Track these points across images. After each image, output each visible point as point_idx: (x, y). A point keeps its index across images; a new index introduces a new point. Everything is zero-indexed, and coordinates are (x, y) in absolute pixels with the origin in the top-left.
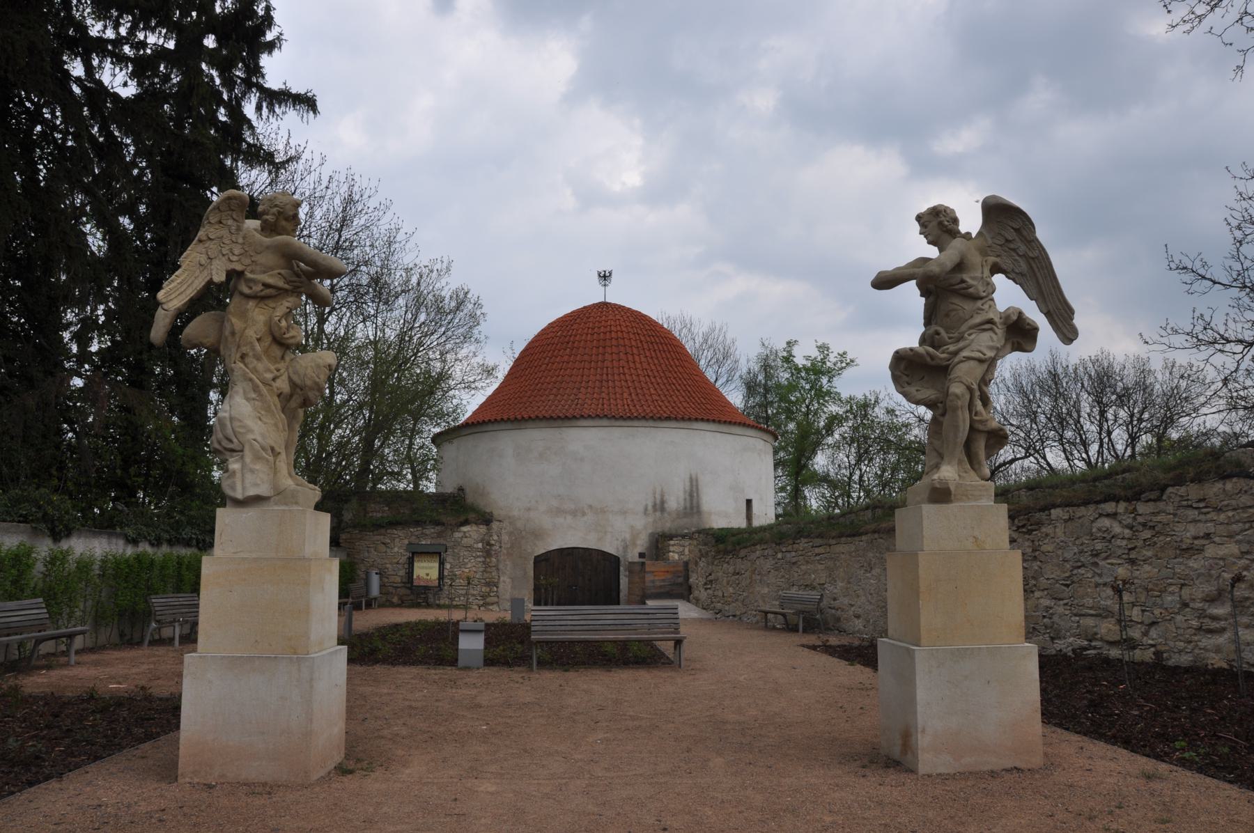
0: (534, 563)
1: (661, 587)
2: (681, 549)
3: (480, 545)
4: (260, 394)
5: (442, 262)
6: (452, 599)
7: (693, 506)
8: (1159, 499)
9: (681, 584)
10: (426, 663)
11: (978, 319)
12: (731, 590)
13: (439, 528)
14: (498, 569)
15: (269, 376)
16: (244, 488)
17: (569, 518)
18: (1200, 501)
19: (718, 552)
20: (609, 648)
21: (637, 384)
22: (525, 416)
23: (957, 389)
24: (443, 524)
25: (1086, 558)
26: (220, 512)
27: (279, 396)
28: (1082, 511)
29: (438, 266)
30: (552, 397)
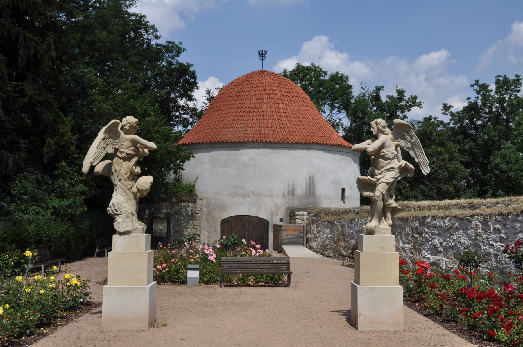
0: (221, 224)
1: (291, 238)
7: (311, 191)
11: (388, 167)
14: (200, 227)
15: (129, 187)
17: (241, 198)
22: (216, 140)
26: (114, 236)
27: (133, 193)
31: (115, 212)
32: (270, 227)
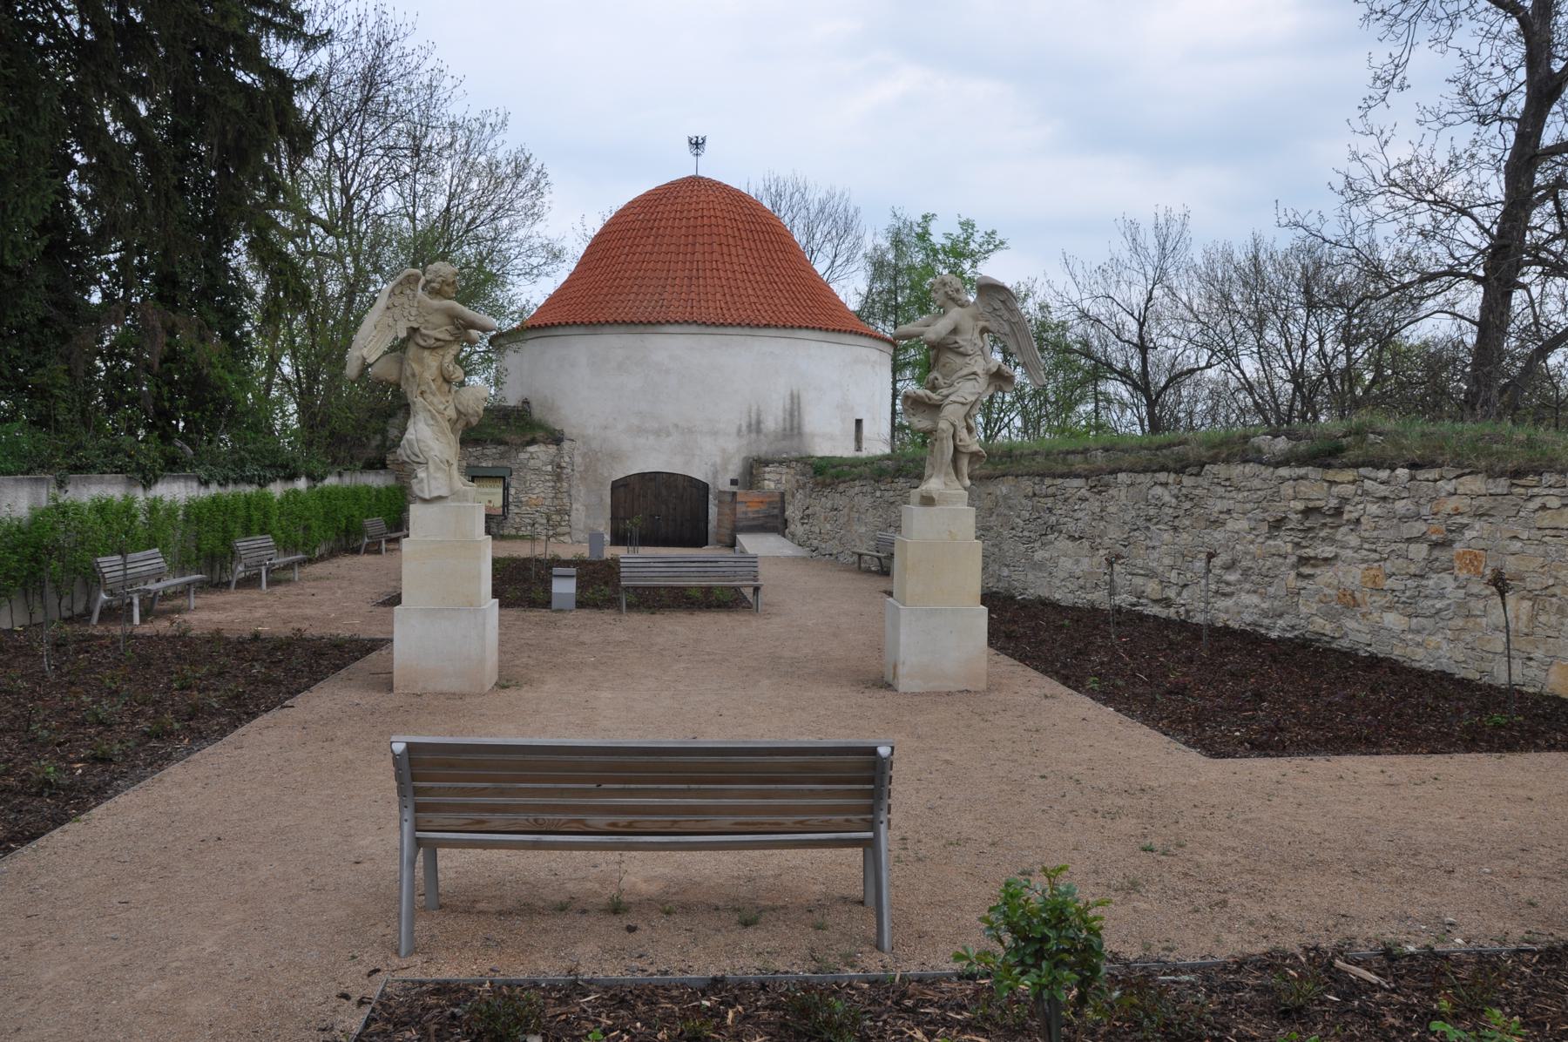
1: (754, 519)
2: (778, 477)
3: (549, 468)
4: (437, 421)
5: (497, 114)
6: (518, 529)
7: (793, 427)
8: (1198, 475)
9: (776, 516)
10: (519, 605)
11: (965, 371)
12: (828, 527)
13: (502, 448)
15: (442, 407)
16: (430, 491)
18: (1227, 480)
19: (817, 484)
20: (692, 593)
21: (732, 282)
23: (943, 425)
24: (506, 443)
25: (1141, 523)
26: (412, 507)
28: (1141, 478)
29: (492, 119)
30: (632, 296)
31: (413, 458)
32: (710, 497)
